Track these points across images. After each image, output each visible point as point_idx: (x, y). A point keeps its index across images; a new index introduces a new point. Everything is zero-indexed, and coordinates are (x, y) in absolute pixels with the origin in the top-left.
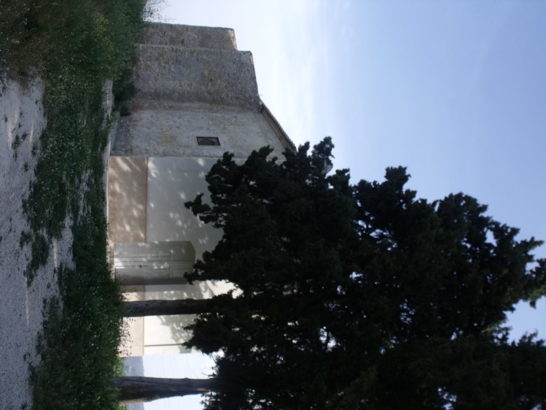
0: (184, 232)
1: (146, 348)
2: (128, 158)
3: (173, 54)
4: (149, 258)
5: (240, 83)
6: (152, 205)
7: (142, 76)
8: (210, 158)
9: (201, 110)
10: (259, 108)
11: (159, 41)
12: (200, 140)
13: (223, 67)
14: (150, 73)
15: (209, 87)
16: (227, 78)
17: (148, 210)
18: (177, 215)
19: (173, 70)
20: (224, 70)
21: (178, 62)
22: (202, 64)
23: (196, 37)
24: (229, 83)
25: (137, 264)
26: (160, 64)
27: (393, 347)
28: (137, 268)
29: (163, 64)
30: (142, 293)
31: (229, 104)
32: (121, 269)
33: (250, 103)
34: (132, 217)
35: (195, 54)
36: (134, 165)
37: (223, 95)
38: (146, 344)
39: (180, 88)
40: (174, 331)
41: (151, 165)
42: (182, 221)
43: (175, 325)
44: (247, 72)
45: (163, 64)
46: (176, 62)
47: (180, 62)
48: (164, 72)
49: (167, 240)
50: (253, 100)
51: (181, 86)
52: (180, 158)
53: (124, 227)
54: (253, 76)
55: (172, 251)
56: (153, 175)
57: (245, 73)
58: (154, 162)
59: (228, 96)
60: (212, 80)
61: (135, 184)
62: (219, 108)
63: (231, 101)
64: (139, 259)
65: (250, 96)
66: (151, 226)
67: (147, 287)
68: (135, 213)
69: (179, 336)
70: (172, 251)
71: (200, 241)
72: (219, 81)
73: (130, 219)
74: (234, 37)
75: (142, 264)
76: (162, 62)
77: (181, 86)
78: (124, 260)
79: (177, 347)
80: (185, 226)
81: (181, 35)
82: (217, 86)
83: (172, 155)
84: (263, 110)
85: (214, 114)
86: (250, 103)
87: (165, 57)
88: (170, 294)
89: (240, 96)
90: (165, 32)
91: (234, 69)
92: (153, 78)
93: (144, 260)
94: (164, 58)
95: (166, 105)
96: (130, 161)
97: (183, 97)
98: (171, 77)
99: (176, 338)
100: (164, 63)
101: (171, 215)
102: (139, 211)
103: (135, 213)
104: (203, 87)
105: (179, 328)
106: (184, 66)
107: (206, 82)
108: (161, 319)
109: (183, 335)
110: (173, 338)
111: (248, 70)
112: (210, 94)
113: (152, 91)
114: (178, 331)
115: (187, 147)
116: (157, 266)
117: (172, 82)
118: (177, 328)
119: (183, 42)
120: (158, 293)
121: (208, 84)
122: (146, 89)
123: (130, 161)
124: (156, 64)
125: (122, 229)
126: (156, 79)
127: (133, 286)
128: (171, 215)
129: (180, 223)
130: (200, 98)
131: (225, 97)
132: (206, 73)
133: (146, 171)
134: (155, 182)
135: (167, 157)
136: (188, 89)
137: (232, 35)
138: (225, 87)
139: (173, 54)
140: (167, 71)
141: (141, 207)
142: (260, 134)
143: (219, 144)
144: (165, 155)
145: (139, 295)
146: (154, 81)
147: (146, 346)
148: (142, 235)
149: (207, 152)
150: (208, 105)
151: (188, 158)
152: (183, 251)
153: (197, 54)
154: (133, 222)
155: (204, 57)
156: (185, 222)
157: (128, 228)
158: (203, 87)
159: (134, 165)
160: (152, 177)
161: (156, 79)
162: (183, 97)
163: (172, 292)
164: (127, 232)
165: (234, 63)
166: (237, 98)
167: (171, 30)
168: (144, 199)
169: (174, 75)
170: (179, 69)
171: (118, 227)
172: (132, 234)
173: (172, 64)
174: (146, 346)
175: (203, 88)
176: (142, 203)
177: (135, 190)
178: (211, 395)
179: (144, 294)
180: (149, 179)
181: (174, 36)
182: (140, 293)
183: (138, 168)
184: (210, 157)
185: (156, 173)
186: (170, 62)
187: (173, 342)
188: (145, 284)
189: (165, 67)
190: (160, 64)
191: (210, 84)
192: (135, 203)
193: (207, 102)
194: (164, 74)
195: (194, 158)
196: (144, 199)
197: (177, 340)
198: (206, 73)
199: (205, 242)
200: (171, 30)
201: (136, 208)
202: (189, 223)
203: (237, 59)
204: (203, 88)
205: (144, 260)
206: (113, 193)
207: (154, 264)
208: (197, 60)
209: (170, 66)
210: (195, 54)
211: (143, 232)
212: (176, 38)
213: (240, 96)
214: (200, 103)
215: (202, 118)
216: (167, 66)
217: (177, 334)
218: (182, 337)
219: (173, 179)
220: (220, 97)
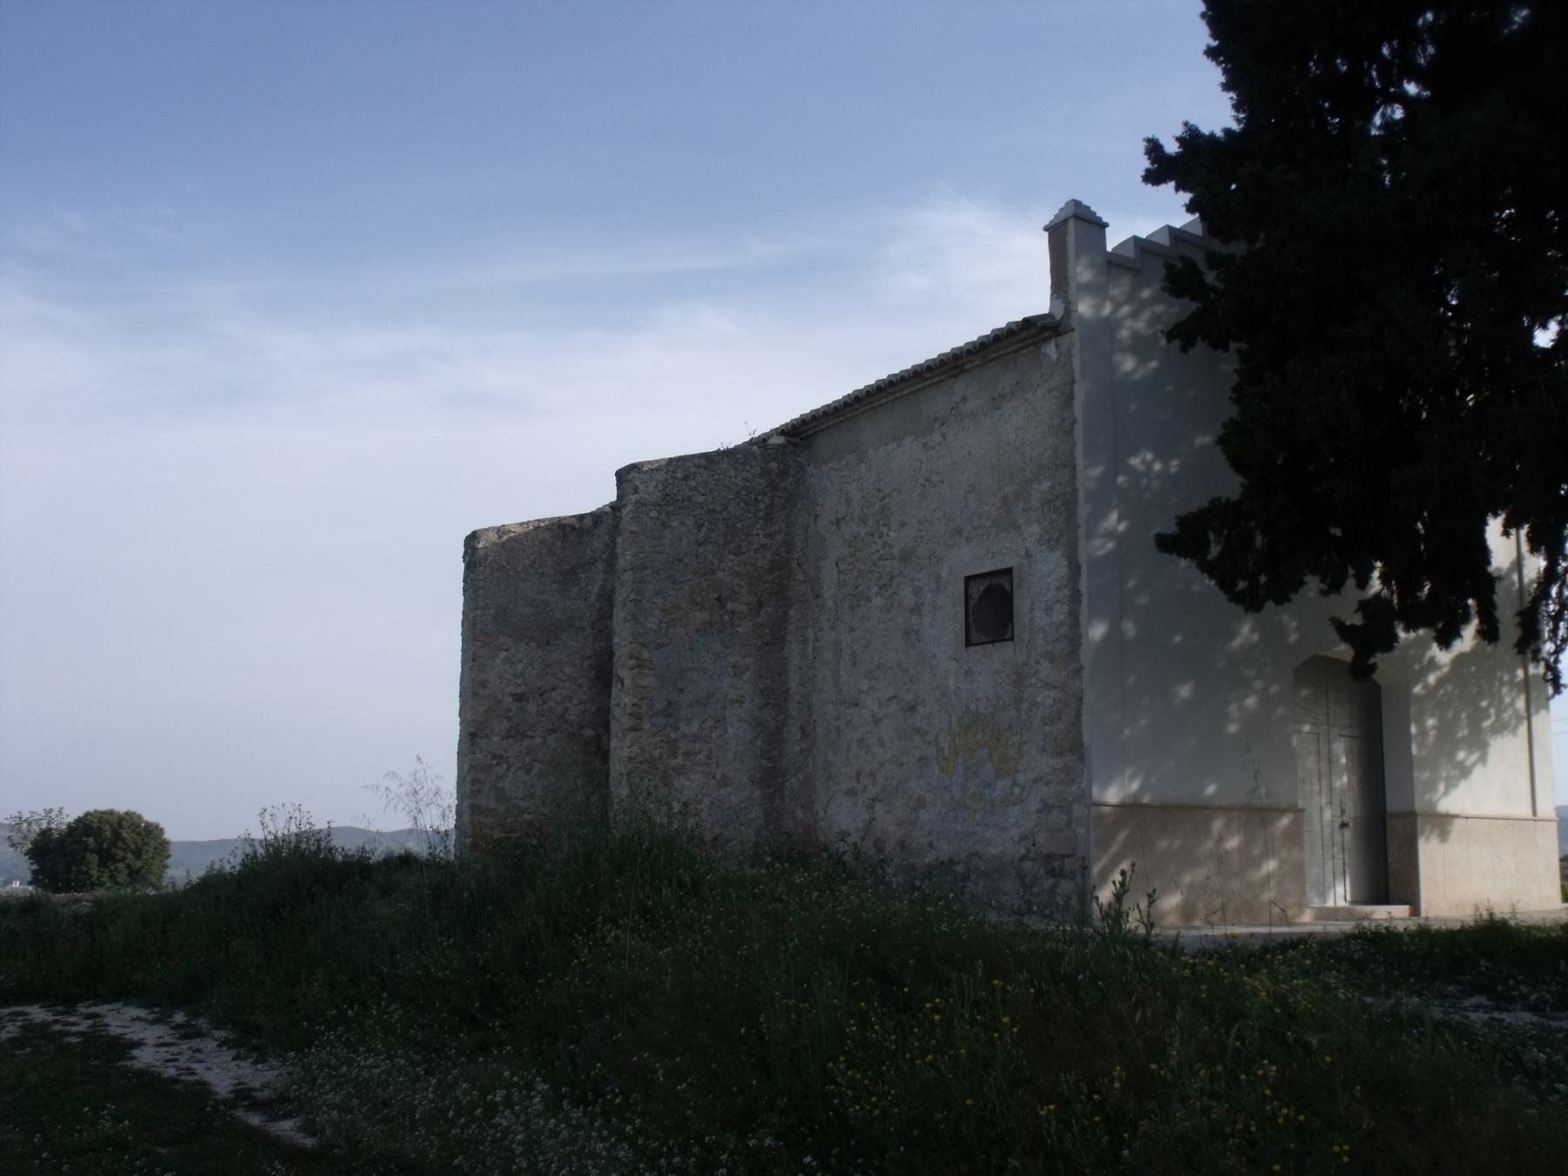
0: (1274, 689)
1: (1540, 814)
2: (1096, 869)
3: (647, 726)
5: (726, 507)
7: (717, 830)
8: (1085, 600)
9: (810, 634)
10: (795, 445)
11: (519, 773)
12: (975, 637)
13: (680, 561)
14: (707, 800)
15: (739, 607)
16: (709, 547)
17: (1224, 802)
18: (1233, 708)
19: (695, 727)
20: (686, 560)
21: (670, 709)
22: (671, 631)
23: (503, 654)
24: (727, 543)
26: (679, 771)
29: (679, 761)
30: (1420, 821)
31: (788, 545)
32: (1352, 887)
33: (783, 474)
34: (1243, 849)
35: (645, 654)
36: (1113, 850)
37: (763, 563)
38: (1526, 811)
39: (746, 705)
40: (1500, 728)
41: (1112, 795)
42: (1246, 696)
43: (1486, 724)
44: (693, 483)
45: (679, 761)
46: (669, 715)
47: (670, 703)
48: (701, 757)
50: (773, 465)
51: (740, 701)
52: (1089, 698)
53: (1269, 876)
54: (703, 462)
56: (1135, 786)
57: (694, 489)
58: (1106, 785)
59: (764, 547)
60: (719, 599)
61: (1162, 844)
62: (800, 577)
63: (779, 538)
64: (1327, 830)
65: (761, 476)
67: (1392, 804)
68: (1233, 843)
69: (1509, 712)
72: (720, 575)
74: (500, 531)
76: (674, 762)
77: (740, 701)
78: (1329, 879)
79: (1535, 720)
80: (1258, 685)
81: (499, 702)
82: (737, 580)
83: (1077, 721)
84: (803, 434)
85: (828, 592)
86: (783, 474)
87: (656, 753)
88: (1418, 734)
89: (762, 506)
90: (494, 756)
91: (683, 523)
92: (723, 791)
94: (661, 757)
95: (797, 749)
96: (1104, 861)
97: (774, 696)
98: (714, 735)
99: (1513, 722)
100: (674, 754)
104: (740, 630)
105: (1492, 711)
106: (682, 690)
107: (726, 618)
108: (1474, 764)
109: (1507, 700)
110: (1514, 730)
111: (685, 478)
112: (761, 604)
113: (758, 793)
114: (1499, 713)
115: (1020, 679)
117: (730, 730)
118: (1493, 719)
119: (519, 698)
120: (451, 823)
121: (733, 612)
122: (752, 815)
123: (1104, 861)
124: (679, 782)
125: (1272, 883)
126: (725, 781)
127: (1393, 847)
128: (1233, 728)
129: (1251, 701)
130: (774, 639)
131: (768, 556)
132: (699, 617)
133: (1129, 809)
134: (1153, 780)
135: (1086, 740)
136: (747, 675)
137: (493, 537)
138: (736, 554)
139: (647, 726)
140: (698, 746)
141: (1218, 825)
142: (936, 437)
143: (1008, 572)
144: (1076, 748)
146: (729, 790)
147: (1534, 813)
148: (1285, 821)
149: (1048, 610)
150: (792, 612)
151: (1086, 673)
153: (645, 646)
154: (1257, 851)
155: (651, 624)
157: (1271, 865)
158: (740, 630)
159: (1113, 850)
160: (1142, 790)
161: (725, 781)
162: (774, 696)
163: (1413, 729)
164: (1280, 867)
165: (665, 525)
166: (768, 518)
167: (487, 737)
168: (1193, 814)
169: (710, 723)
170: (690, 706)
171: (1267, 896)
173: (677, 729)
174: (1534, 813)
175: (743, 628)
176: (1207, 822)
177: (1177, 843)
180: (1146, 799)
181: (505, 725)
182: (1419, 829)
183: (1121, 837)
184: (1075, 598)
185: (1132, 778)
186: (673, 735)
187: (1523, 729)
188: (1385, 812)
189: (688, 754)
190: (679, 771)
191: (729, 606)
192: (1210, 844)
193: (785, 613)
194: (708, 757)
195: (1086, 656)
196: (1193, 814)
197: (1519, 719)
198: (699, 617)
199: (1294, 624)
200: (487, 737)
201: (1221, 840)
202: (1251, 673)
203: (654, 514)
204: (743, 628)
205: (1328, 814)
206: (1187, 912)
207: (1337, 784)
208: (660, 646)
209: (684, 736)
210: (645, 654)
211: (1278, 819)
212: (509, 719)
213: (762, 506)
214: (789, 637)
215: (852, 630)
216: (683, 747)
217: (1506, 716)
218: (1512, 703)
219: (1143, 722)
220: (770, 571)
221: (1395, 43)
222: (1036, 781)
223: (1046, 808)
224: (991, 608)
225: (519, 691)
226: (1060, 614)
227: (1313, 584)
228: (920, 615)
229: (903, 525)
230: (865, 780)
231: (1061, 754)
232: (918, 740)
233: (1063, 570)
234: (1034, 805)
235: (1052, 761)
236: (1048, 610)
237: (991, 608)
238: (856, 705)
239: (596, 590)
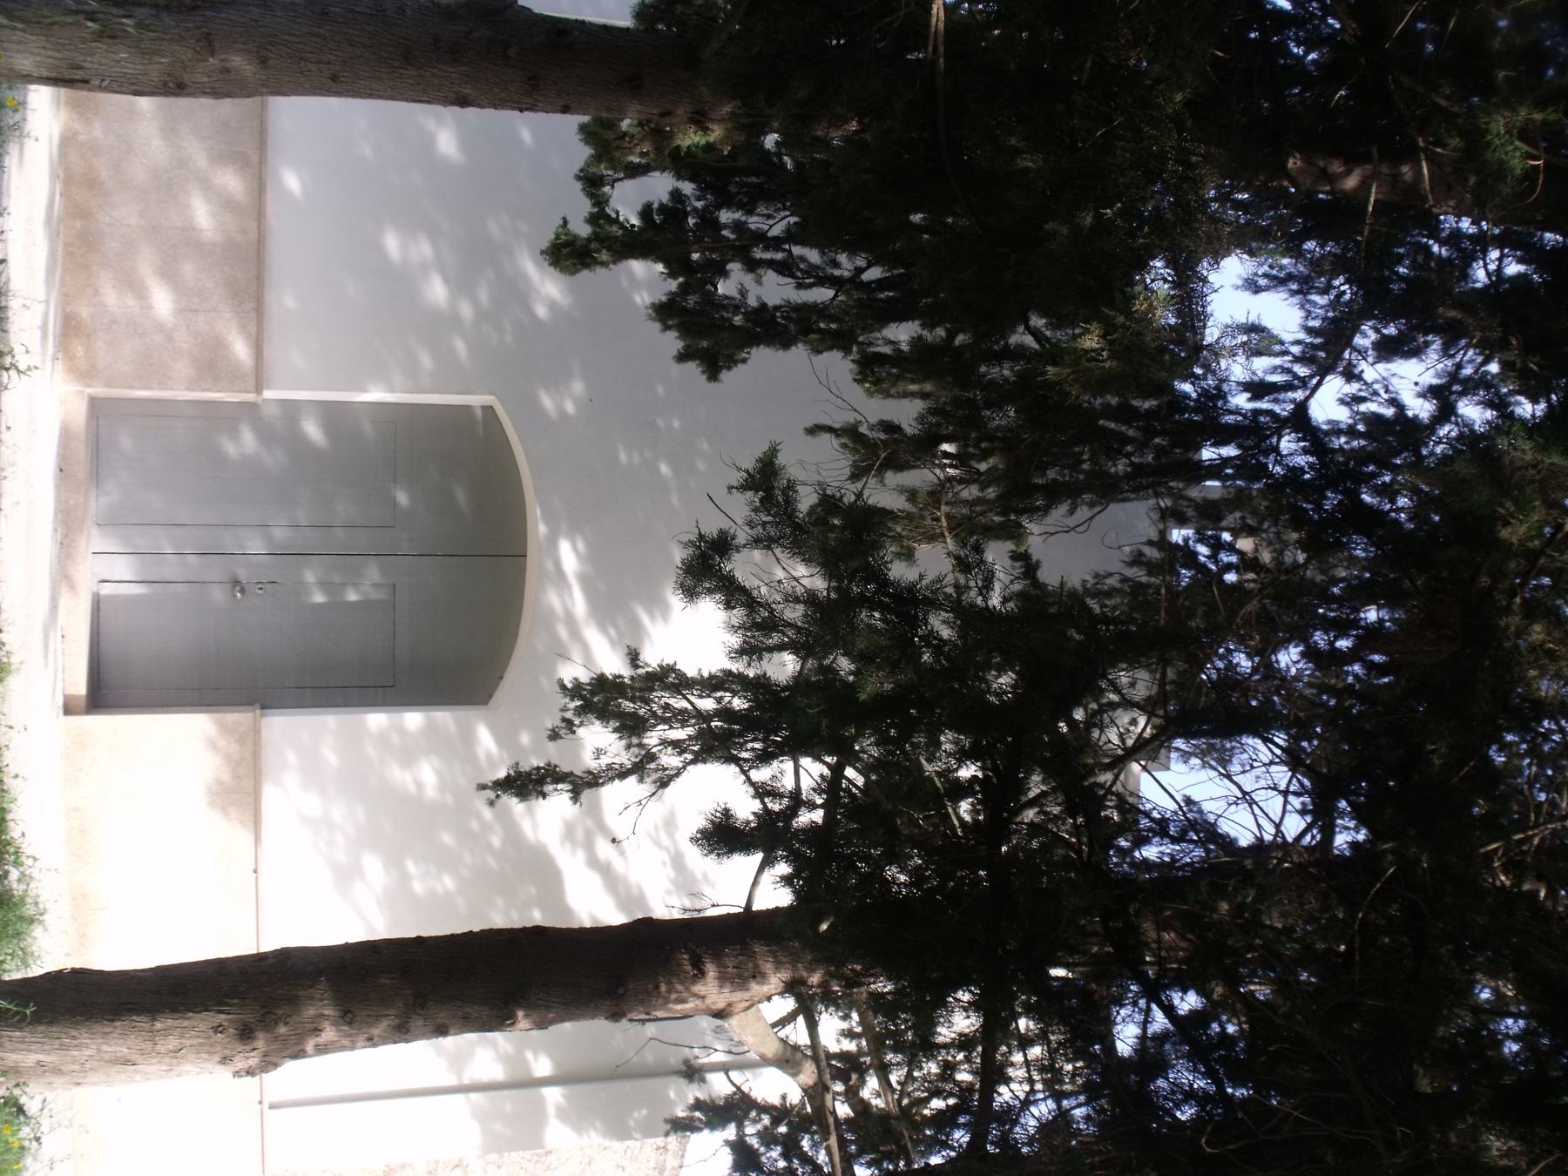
0: (460, 346)
4: (279, 534)
6: (292, 181)
18: (424, 249)
25: (216, 570)
27: (1515, 1048)
28: (219, 595)
34: (189, 240)
42: (446, 280)
49: (375, 395)
53: (141, 293)
55: (402, 498)
66: (285, 300)
70: (402, 498)
71: (547, 402)
73: (177, 247)
75: (243, 575)
80: (466, 310)
88: (402, 732)
93: (256, 545)
101: (392, 243)
102: (226, 204)
103: (203, 216)
116: (325, 585)
125: (131, 302)
128: (392, 243)
129: (437, 291)
141: (231, 182)
145: (225, 730)
148: (241, 349)
152: (461, 496)
154: (188, 269)
156: (461, 284)
157: (162, 302)
164: (160, 327)
172: (183, 340)
178: (854, 282)
179: (257, 731)
201: (206, 186)
202: (483, 295)
205: (256, 545)
211: (243, 327)
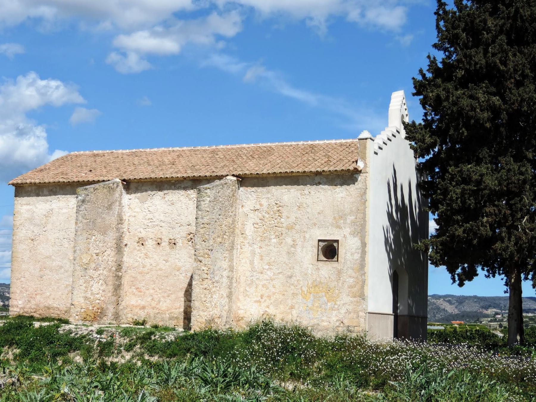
143: (337, 241)
221: (466, 265)
222: (344, 304)
223: (348, 312)
224: (330, 251)
225: (97, 252)
226: (357, 256)
227: (438, 227)
228: (295, 248)
229: (288, 217)
230: (265, 298)
231: (355, 297)
232: (292, 287)
233: (359, 243)
234: (343, 311)
235: (351, 299)
236: (352, 254)
237: (330, 251)
238: (262, 273)
239: (116, 213)
